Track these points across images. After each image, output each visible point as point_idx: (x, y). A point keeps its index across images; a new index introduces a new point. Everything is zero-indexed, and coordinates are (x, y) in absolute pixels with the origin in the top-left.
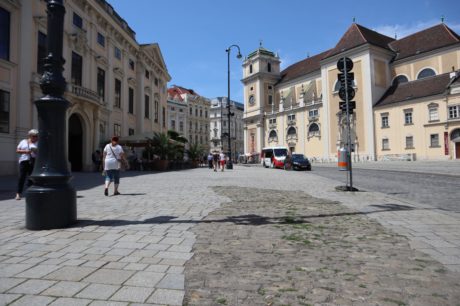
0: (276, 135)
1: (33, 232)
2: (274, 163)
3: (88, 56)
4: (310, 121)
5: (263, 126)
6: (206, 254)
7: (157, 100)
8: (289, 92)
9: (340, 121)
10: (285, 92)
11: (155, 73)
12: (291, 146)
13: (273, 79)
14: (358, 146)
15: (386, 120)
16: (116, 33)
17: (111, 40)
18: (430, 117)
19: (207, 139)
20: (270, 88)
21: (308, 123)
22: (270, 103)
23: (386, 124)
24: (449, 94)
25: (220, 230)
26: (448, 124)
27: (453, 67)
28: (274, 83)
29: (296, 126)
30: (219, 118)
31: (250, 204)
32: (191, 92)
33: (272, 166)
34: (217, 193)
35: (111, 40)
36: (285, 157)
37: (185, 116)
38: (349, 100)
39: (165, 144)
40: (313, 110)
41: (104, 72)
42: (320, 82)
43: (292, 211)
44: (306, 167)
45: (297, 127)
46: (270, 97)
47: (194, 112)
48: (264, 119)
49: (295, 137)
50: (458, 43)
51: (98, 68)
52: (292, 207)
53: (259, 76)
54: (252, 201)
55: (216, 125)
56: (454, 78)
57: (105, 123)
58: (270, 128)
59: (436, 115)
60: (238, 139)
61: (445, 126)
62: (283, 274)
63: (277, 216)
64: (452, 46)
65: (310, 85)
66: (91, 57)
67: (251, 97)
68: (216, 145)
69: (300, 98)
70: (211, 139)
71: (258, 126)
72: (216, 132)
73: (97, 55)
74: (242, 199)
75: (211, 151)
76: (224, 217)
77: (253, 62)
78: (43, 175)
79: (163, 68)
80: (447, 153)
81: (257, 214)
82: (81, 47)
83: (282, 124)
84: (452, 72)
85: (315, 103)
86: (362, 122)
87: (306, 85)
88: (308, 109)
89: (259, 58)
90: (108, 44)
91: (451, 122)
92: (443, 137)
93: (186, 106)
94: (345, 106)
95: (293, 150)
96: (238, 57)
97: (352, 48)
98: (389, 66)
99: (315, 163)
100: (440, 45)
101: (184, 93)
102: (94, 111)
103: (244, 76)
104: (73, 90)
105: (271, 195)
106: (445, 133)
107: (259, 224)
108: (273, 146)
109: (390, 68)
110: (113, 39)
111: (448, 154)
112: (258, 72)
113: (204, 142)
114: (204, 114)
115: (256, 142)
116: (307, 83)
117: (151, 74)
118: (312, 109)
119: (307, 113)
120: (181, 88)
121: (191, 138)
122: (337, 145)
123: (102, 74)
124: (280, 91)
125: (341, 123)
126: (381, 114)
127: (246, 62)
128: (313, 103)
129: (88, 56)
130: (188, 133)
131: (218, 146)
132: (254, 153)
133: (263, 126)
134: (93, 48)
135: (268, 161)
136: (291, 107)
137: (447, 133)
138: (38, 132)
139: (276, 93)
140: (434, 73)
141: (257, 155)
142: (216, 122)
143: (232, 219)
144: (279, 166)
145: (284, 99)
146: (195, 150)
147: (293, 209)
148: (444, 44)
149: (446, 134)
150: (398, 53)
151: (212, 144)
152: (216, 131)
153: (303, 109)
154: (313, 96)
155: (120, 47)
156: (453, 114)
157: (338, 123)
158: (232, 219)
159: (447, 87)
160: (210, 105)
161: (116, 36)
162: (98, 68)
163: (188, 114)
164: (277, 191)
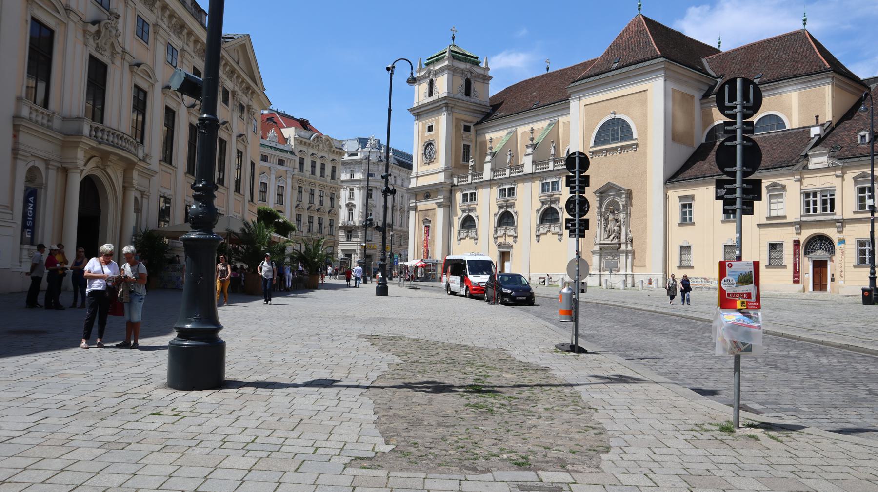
0: (474, 226)
1: (184, 393)
2: (467, 287)
3: (118, 61)
4: (543, 203)
5: (449, 206)
6: (390, 416)
7: (242, 149)
8: (505, 140)
9: (601, 206)
10: (497, 139)
11: (241, 93)
12: (502, 250)
13: (474, 111)
14: (634, 257)
15: (688, 209)
16: (172, 16)
17: (161, 30)
18: (770, 210)
19: (331, 225)
20: (467, 129)
21: (538, 205)
22: (466, 158)
23: (688, 217)
24: (805, 168)
25: (396, 396)
26: (800, 225)
27: (817, 117)
28: (475, 120)
29: (515, 210)
30: (360, 181)
31: (427, 367)
32: (304, 124)
33: (463, 293)
34: (376, 348)
35: (161, 31)
36: (488, 276)
37: (289, 175)
38: (580, 216)
39: (264, 244)
40: (550, 181)
41: (145, 93)
42: (567, 125)
43: (482, 378)
44: (525, 298)
45: (516, 213)
46: (467, 148)
47: (308, 166)
48: (451, 192)
49: (512, 233)
50: (828, 70)
51: (136, 86)
52: (484, 373)
53: (447, 104)
54: (430, 363)
55: (351, 195)
56: (817, 138)
57: (142, 193)
58: (464, 211)
59: (781, 206)
60: (396, 227)
61: (796, 229)
62: (463, 431)
63: (463, 384)
64: (817, 76)
65: (547, 129)
66: (123, 65)
67: (429, 145)
68: (349, 237)
69: (526, 155)
70: (340, 225)
71: (439, 205)
72: (351, 210)
73: (135, 61)
74: (416, 358)
75: (340, 248)
76: (399, 383)
77: (436, 73)
78: (189, 326)
79: (255, 83)
80: (796, 280)
81: (438, 380)
82: (108, 47)
83: (487, 205)
84: (814, 126)
85: (554, 166)
86: (644, 210)
87: (539, 129)
88: (540, 177)
89: (447, 67)
90: (155, 38)
91: (806, 221)
92: (792, 248)
93: (292, 153)
94: (574, 225)
95: (506, 258)
96: (408, 82)
97: (631, 64)
98: (702, 104)
99: (549, 286)
100: (797, 72)
101: (289, 126)
102: (125, 171)
103: (416, 100)
104: (91, 131)
105: (457, 354)
106: (795, 241)
107: (441, 392)
108: (464, 251)
109: (702, 108)
110: (165, 27)
111: (798, 282)
112: (445, 95)
113: (326, 231)
114: (328, 171)
115: (433, 237)
116: (541, 126)
117: (233, 97)
118: (549, 178)
119: (537, 185)
120: (282, 114)
121: (298, 220)
122: (594, 253)
123: (141, 97)
124: (488, 137)
125: (603, 210)
126: (680, 197)
127: (422, 74)
128: (551, 166)
129: (118, 61)
130: (294, 209)
131: (353, 239)
132: (428, 260)
133: (449, 205)
134: (127, 48)
135: (455, 282)
136: (508, 171)
137: (799, 241)
138: (112, 247)
139: (479, 139)
140: (782, 124)
141: (435, 264)
142: (352, 190)
143: (408, 386)
144: (476, 293)
145: (493, 155)
146: (315, 255)
147: (485, 376)
148: (803, 71)
149: (797, 243)
150: (719, 80)
151: (342, 236)
152: (350, 207)
153: (531, 177)
154: (552, 152)
155: (177, 43)
156: (811, 207)
157: (596, 210)
158: (408, 386)
159: (804, 154)
160: (342, 154)
161: (170, 22)
162: (136, 86)
163: (296, 171)
164: (467, 348)
